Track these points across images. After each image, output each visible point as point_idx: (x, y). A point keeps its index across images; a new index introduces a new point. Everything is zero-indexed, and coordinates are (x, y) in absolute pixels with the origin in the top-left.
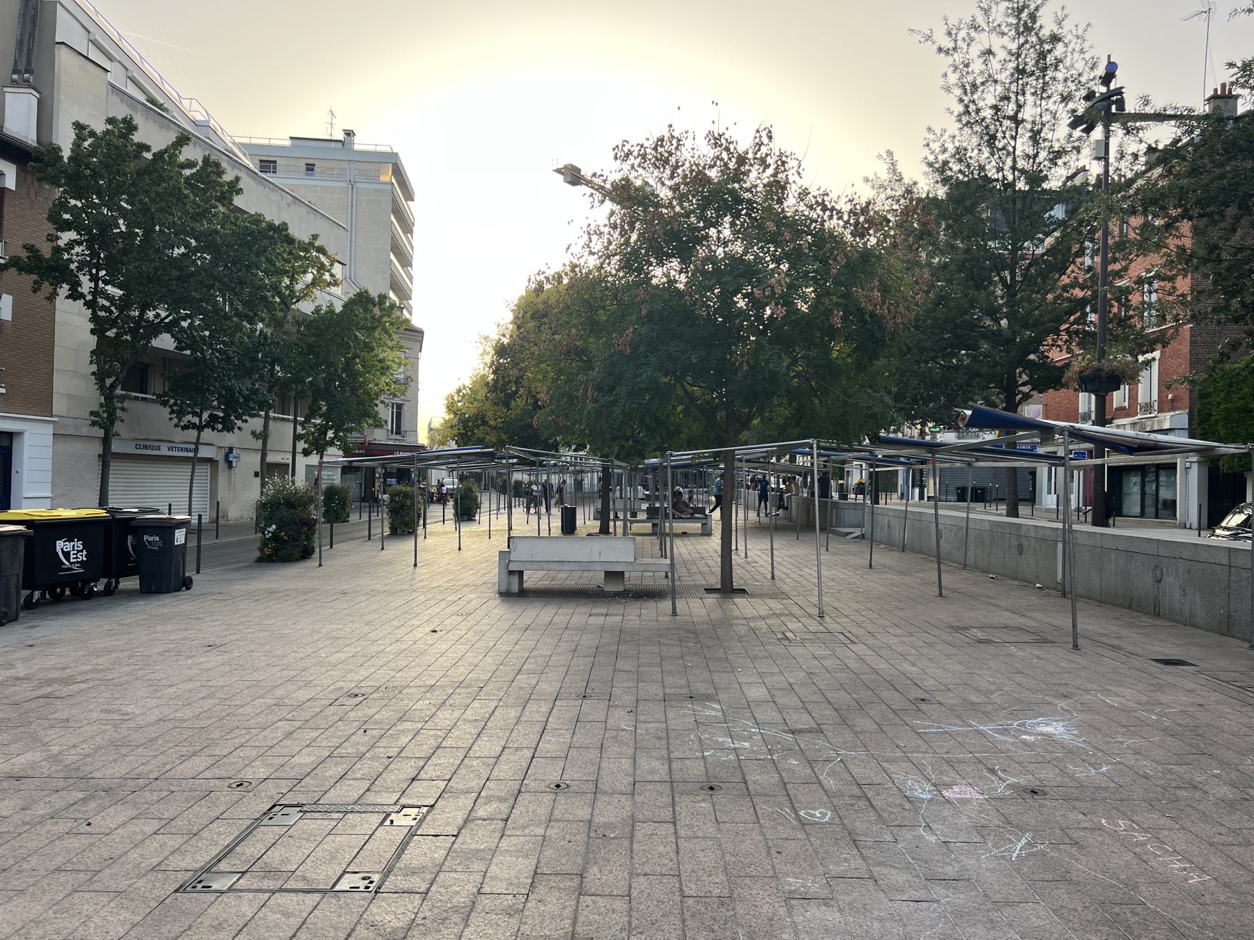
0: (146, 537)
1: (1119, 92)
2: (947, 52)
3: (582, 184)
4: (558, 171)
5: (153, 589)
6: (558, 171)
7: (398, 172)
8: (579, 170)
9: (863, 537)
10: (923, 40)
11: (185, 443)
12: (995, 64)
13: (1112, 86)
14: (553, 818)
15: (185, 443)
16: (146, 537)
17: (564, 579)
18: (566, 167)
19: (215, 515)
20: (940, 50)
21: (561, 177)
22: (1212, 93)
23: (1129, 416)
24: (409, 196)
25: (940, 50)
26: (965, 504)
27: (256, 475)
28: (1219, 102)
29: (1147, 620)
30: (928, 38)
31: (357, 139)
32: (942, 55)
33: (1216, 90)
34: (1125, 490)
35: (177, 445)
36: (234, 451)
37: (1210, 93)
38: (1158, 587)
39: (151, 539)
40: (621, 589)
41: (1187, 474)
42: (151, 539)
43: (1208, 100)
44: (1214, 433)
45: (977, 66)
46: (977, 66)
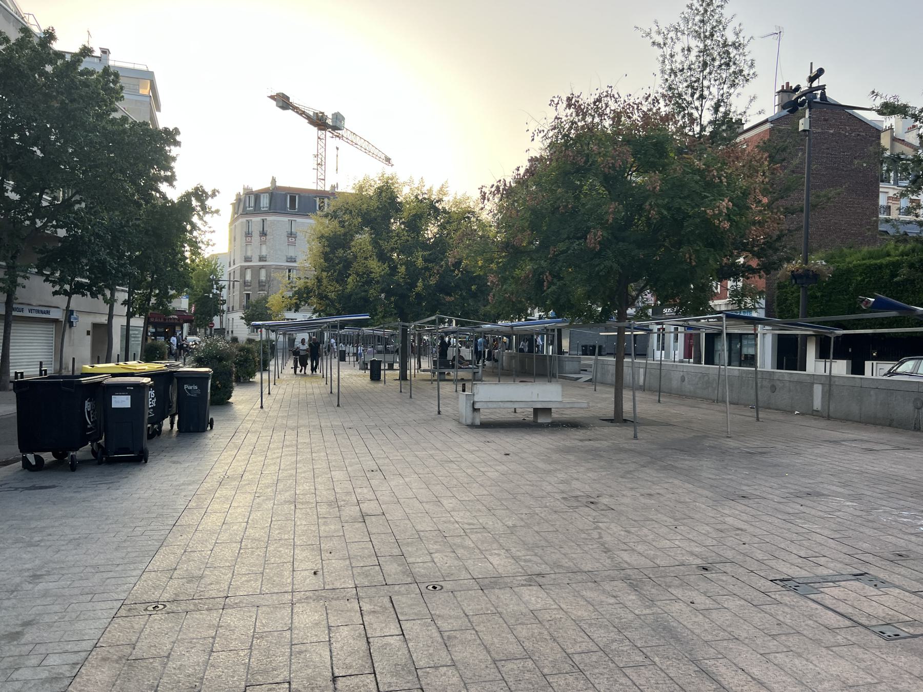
0: (186, 387)
1: (822, 88)
2: (659, 45)
3: (289, 109)
4: (272, 97)
5: (191, 428)
6: (272, 97)
7: (153, 88)
8: (288, 98)
9: (590, 380)
10: (644, 35)
11: (40, 306)
12: (692, 57)
13: (815, 84)
14: (455, 593)
15: (40, 306)
16: (186, 387)
17: (504, 415)
18: (278, 95)
19: (58, 367)
20: (654, 43)
21: (274, 103)
22: (780, 89)
23: (721, 299)
24: (159, 109)
25: (654, 43)
26: (593, 357)
27: (88, 333)
28: (785, 94)
29: (911, 432)
30: (648, 34)
31: (111, 57)
32: (656, 47)
33: (783, 86)
34: (716, 349)
35: (35, 308)
36: (75, 314)
37: (779, 88)
38: (918, 412)
39: (190, 388)
40: (549, 420)
41: (764, 337)
42: (190, 388)
43: (778, 92)
44: (789, 311)
45: (679, 58)
46: (679, 58)
